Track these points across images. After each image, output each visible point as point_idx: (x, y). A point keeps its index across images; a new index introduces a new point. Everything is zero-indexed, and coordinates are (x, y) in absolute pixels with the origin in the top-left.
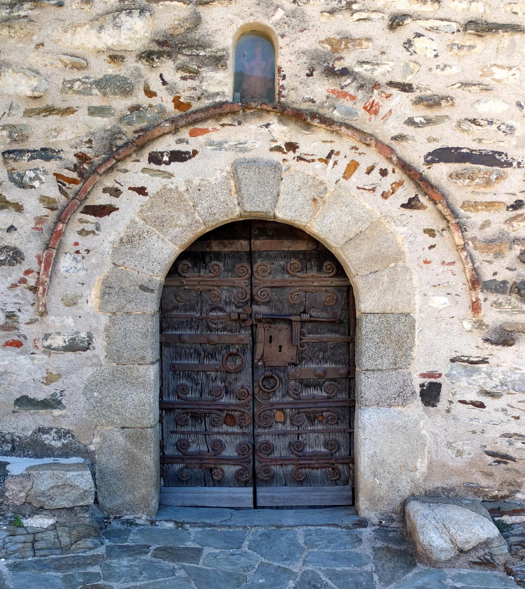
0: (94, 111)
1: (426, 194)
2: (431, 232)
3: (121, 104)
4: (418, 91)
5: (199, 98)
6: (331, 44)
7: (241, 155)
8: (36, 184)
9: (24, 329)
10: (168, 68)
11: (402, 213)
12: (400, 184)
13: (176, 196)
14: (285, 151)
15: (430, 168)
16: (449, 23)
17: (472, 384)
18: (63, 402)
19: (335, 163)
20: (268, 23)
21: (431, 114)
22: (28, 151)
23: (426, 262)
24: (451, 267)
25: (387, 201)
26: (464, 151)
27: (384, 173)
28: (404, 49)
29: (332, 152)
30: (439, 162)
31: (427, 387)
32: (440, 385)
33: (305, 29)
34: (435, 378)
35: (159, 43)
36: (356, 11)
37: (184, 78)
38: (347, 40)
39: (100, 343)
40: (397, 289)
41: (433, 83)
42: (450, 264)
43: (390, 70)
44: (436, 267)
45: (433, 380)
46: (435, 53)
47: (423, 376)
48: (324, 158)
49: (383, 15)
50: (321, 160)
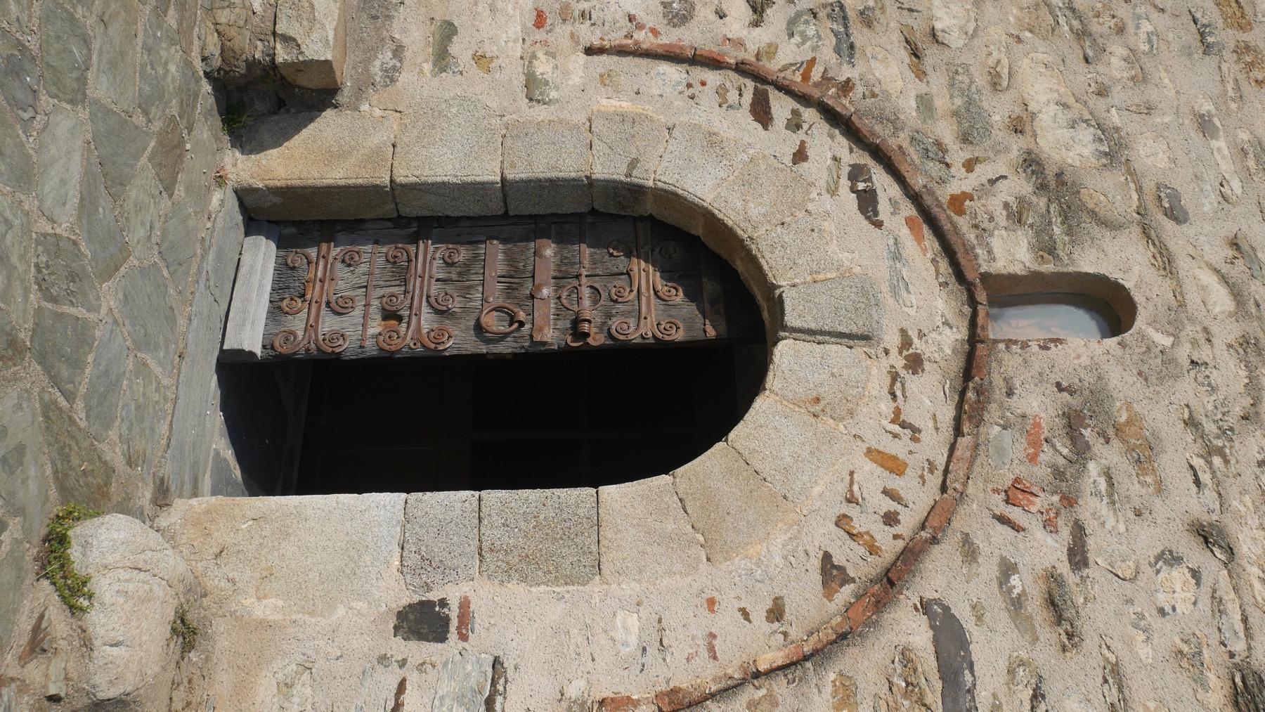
0: (925, 103)
1: (859, 597)
2: (776, 613)
3: (945, 131)
4: (1078, 580)
5: (976, 226)
6: (1129, 422)
7: (885, 288)
8: (797, 39)
9: (562, 32)
10: (1018, 186)
11: (812, 554)
12: (873, 550)
13: (799, 198)
14: (905, 353)
15: (916, 609)
16: (1242, 635)
17: (442, 705)
18: (444, 74)
19: (895, 436)
20: (1140, 323)
21: (1035, 607)
22: (846, 27)
23: (711, 603)
24: (704, 652)
25: (833, 527)
26: (968, 677)
27: (890, 519)
28: (1158, 551)
29: (915, 430)
30: (932, 627)
31: (439, 613)
32: (442, 638)
33: (1146, 380)
34: (458, 628)
35: (1059, 175)
36: (1210, 463)
37: (1006, 205)
38: (1144, 456)
39: (541, 113)
40: (648, 549)
41: (1100, 607)
42: (712, 650)
43: (1108, 526)
44: (701, 623)
45: (454, 623)
46: (1168, 609)
47: (465, 605)
48: (902, 417)
49: (1218, 511)
50: (897, 412)
